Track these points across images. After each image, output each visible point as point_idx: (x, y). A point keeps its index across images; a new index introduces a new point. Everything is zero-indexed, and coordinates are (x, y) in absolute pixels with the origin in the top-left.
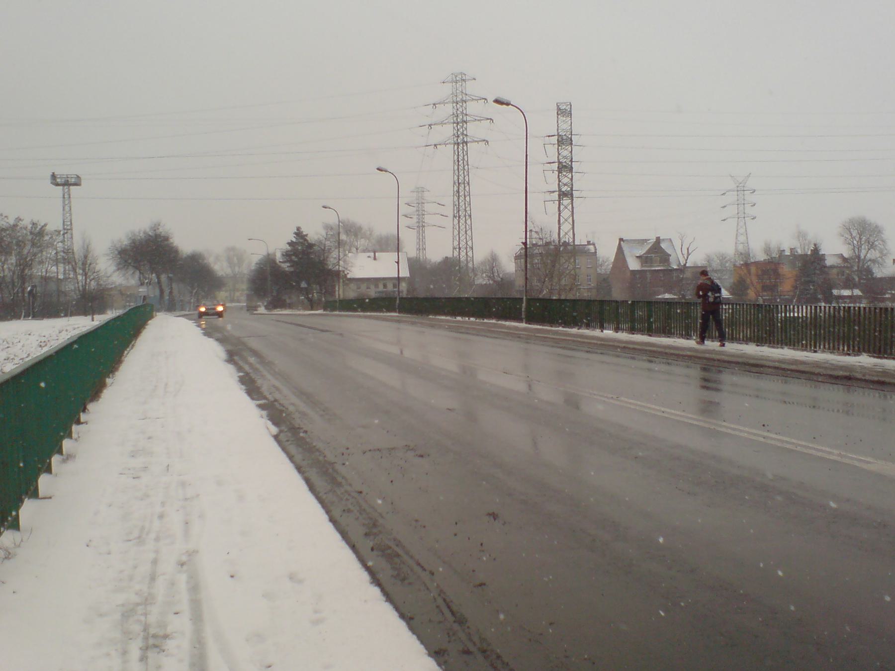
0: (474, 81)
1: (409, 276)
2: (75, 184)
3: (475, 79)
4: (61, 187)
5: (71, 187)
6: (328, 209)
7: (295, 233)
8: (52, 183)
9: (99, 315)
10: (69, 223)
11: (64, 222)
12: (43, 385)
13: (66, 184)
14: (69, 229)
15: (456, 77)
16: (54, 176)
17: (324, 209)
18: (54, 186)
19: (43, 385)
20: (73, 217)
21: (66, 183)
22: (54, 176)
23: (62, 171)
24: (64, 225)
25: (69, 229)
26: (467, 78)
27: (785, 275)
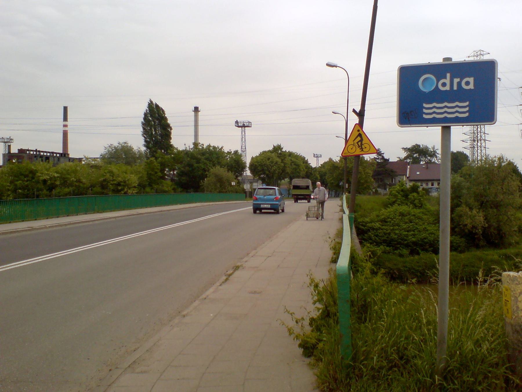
0: (489, 54)
1: (473, 78)
2: (248, 126)
3: (489, 53)
4: (241, 128)
5: (246, 128)
6: (337, 114)
7: (236, 122)
8: (236, 126)
9: (180, 204)
10: (244, 148)
11: (242, 147)
12: (418, 173)
13: (244, 126)
14: (245, 151)
15: (477, 53)
16: (237, 122)
17: (333, 114)
18: (237, 128)
19: (418, 173)
20: (247, 144)
21: (243, 126)
22: (237, 122)
23: (242, 119)
24: (242, 148)
25: (245, 151)
26: (484, 53)
27: (396, 172)
